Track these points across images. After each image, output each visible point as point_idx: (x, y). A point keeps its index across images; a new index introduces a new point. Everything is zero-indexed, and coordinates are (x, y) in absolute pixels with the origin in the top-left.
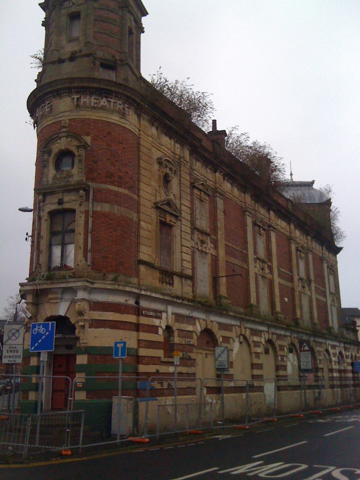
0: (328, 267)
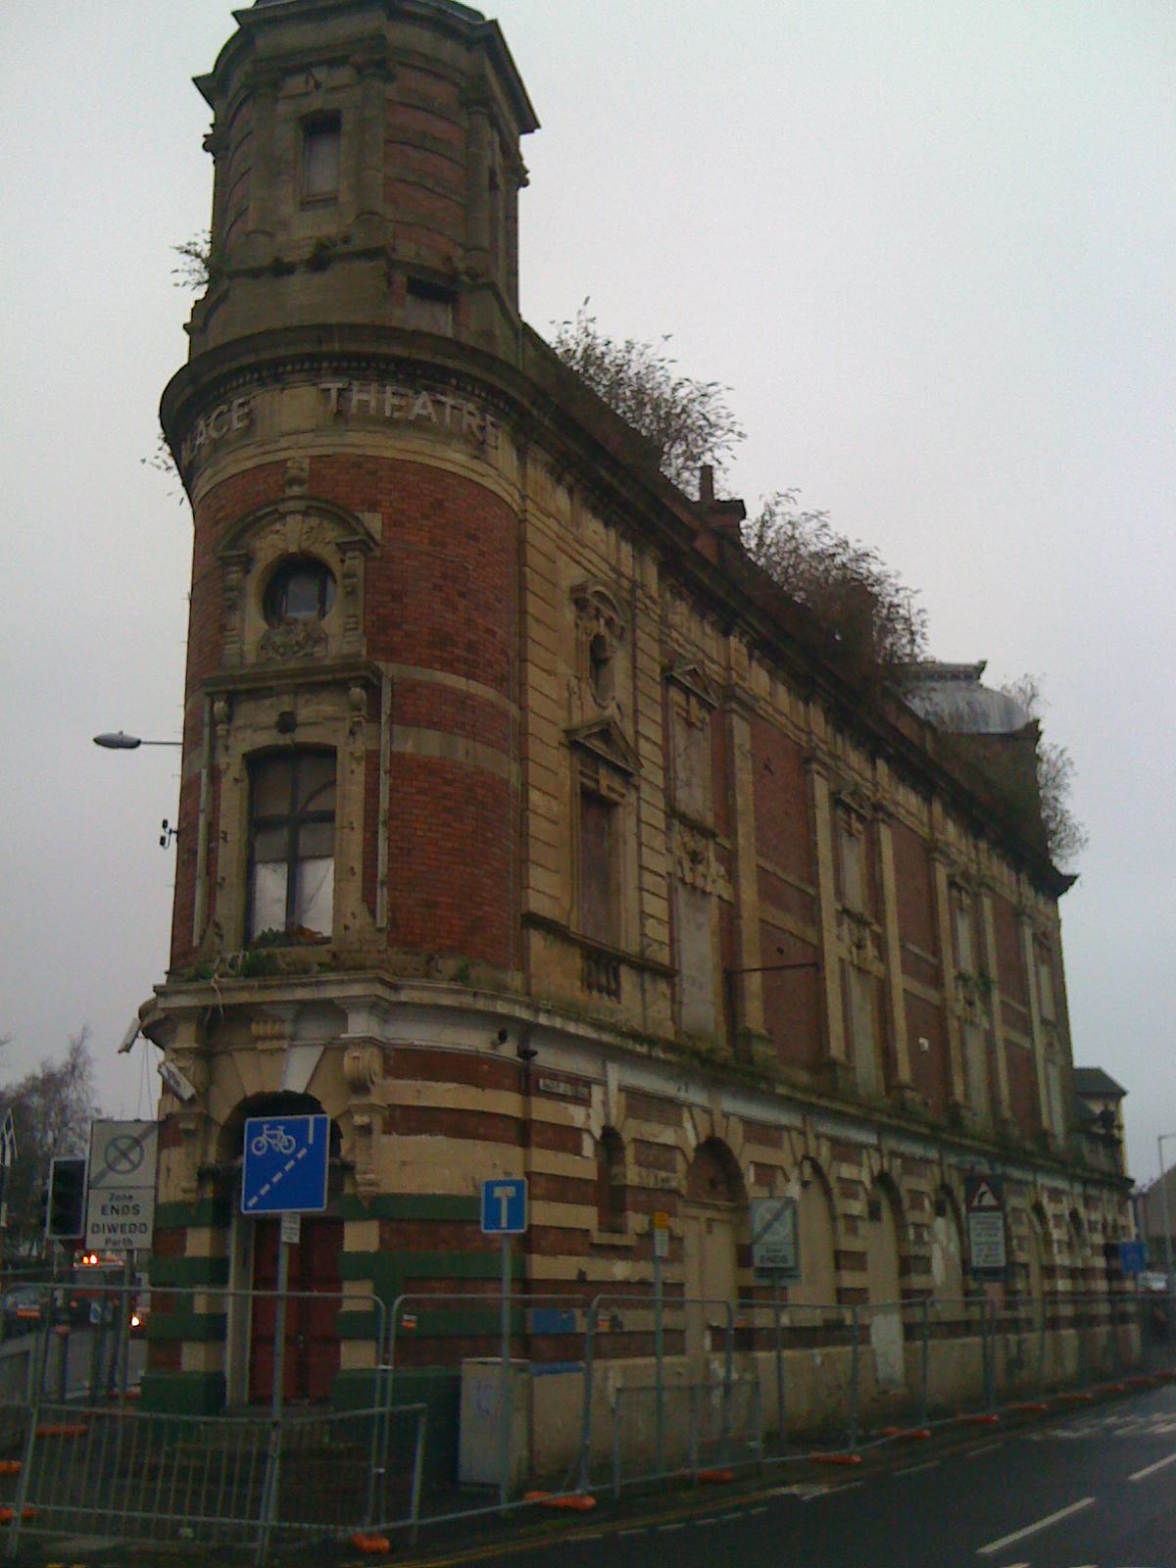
0: (1035, 937)
